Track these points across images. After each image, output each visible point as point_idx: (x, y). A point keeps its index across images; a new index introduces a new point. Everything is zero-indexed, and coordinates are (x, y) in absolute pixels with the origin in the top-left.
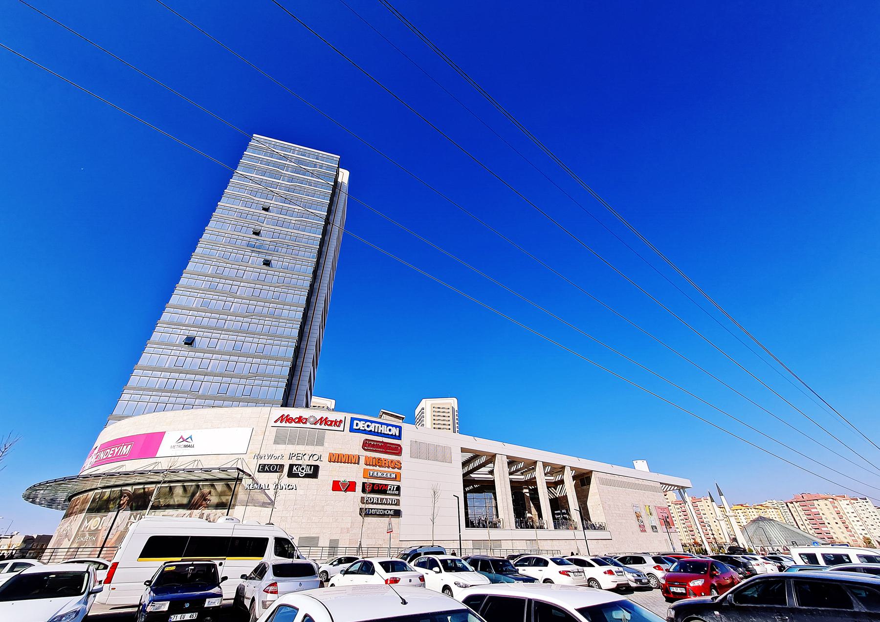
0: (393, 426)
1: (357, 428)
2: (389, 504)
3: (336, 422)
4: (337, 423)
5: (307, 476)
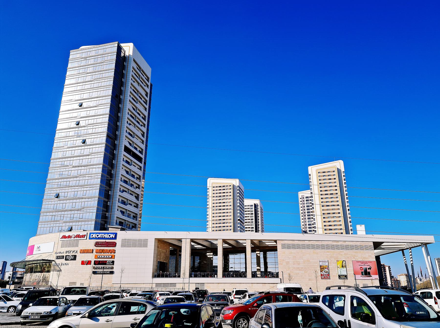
0: (111, 233)
3: (83, 236)
4: (83, 236)
5: (72, 260)
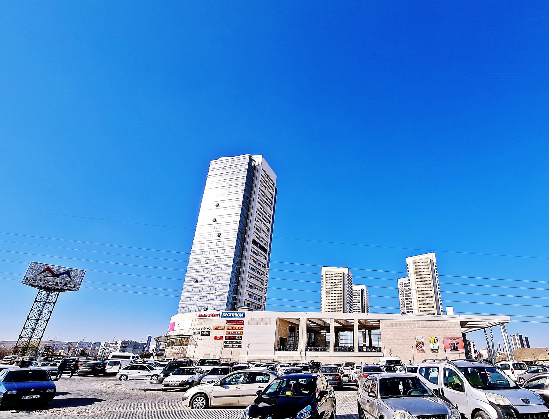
0: (240, 313)
1: (224, 316)
2: (236, 343)
4: (217, 315)
5: (206, 335)
